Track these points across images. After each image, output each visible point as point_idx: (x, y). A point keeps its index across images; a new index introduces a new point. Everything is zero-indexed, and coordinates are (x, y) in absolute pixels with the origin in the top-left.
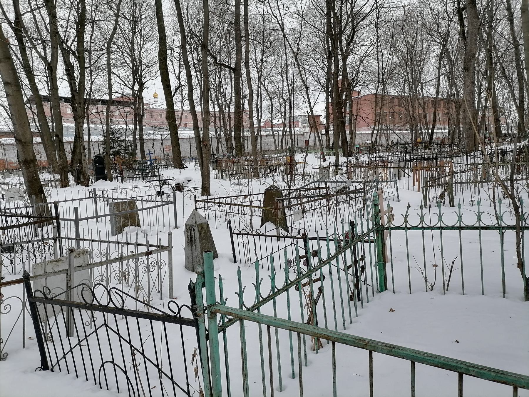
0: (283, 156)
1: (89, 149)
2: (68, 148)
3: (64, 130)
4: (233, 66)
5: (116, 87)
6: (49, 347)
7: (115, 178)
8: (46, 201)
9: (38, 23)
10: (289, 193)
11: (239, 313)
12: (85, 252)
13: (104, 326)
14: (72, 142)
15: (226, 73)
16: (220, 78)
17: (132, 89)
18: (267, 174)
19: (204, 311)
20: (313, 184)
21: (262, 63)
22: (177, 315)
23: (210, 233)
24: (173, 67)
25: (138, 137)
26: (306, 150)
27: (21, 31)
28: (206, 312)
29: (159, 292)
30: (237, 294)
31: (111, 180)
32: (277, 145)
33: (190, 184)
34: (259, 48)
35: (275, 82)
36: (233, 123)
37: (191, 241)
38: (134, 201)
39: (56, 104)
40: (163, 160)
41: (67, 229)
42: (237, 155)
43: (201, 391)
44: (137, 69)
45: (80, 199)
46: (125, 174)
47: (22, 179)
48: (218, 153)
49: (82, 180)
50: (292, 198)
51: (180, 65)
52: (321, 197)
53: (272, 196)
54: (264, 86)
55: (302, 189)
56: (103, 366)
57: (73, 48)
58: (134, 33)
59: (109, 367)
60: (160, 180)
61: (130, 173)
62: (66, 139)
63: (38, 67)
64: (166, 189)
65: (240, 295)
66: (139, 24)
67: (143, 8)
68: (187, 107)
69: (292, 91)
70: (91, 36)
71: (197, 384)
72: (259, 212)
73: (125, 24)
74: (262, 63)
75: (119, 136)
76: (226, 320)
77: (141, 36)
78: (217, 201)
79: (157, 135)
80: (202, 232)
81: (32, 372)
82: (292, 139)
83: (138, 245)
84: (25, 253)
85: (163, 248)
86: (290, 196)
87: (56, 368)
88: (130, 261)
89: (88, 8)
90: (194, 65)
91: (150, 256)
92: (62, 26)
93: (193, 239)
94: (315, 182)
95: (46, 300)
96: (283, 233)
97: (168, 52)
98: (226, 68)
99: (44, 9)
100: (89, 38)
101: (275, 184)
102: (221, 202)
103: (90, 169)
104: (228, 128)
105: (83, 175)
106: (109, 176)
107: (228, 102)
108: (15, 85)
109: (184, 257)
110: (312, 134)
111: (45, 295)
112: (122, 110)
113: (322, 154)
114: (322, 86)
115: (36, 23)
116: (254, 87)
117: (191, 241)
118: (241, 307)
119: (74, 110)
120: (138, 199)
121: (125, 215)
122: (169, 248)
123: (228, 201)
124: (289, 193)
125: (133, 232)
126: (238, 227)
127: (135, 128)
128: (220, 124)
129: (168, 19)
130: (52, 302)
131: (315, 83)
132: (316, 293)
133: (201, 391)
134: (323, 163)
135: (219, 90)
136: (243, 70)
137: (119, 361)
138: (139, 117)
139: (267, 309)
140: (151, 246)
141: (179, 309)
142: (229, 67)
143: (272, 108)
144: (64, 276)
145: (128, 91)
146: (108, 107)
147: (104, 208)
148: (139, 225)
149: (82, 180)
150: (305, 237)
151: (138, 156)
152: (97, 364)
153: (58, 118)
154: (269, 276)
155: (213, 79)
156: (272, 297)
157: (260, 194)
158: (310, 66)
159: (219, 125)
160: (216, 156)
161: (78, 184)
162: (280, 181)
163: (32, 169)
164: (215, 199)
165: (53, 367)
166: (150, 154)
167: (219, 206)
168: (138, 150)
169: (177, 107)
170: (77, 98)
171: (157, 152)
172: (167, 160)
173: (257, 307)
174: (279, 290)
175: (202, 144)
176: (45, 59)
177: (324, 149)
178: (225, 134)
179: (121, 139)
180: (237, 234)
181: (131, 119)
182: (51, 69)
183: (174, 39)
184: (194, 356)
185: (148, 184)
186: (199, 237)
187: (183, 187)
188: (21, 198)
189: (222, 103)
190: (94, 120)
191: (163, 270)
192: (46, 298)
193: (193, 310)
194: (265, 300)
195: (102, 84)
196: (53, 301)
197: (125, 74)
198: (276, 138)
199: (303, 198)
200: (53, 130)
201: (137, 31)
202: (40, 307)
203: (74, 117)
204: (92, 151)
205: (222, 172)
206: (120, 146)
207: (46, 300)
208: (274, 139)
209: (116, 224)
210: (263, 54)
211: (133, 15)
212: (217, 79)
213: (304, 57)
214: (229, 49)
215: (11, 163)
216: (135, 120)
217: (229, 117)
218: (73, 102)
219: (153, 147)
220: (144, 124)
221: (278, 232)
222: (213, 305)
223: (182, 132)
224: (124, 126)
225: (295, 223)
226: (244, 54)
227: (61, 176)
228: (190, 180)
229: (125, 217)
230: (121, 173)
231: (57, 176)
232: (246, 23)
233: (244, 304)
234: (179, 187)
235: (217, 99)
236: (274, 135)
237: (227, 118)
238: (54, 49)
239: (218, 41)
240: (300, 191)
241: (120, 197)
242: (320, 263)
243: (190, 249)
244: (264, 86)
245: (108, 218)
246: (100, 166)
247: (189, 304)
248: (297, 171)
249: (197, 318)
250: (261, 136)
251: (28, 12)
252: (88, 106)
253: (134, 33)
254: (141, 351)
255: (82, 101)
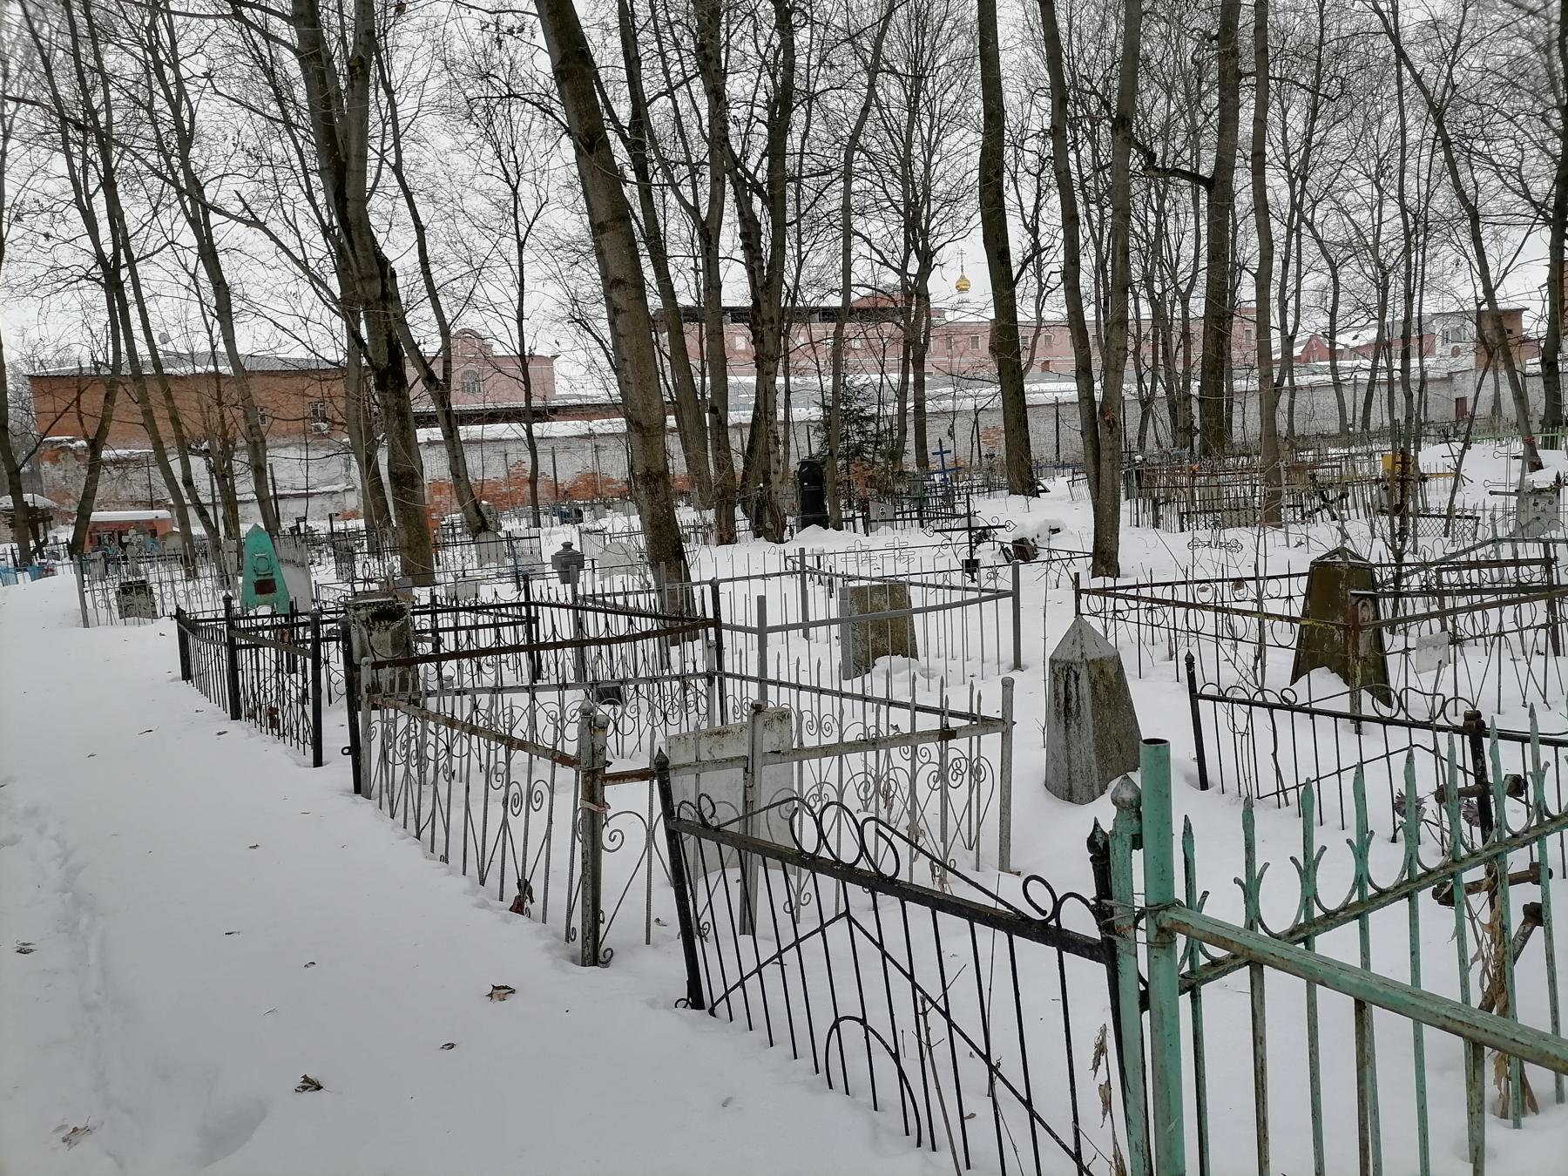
0: (1371, 455)
1: (787, 443)
2: (737, 442)
3: (730, 392)
4: (1205, 171)
5: (861, 270)
6: (707, 951)
7: (847, 520)
8: (688, 578)
9: (683, 120)
10: (1398, 578)
11: (1249, 940)
12: (784, 716)
13: (845, 919)
14: (746, 425)
15: (1182, 195)
16: (1160, 212)
17: (902, 271)
18: (1311, 514)
19: (1137, 920)
20: (1489, 547)
21: (1308, 151)
22: (1050, 919)
23: (1126, 690)
24: (1019, 195)
25: (910, 405)
26: (1464, 427)
27: (643, 146)
28: (1142, 923)
29: (971, 848)
30: (1241, 883)
31: (840, 528)
32: (1349, 416)
33: (1057, 542)
34: (1300, 99)
35: (1354, 204)
36: (1197, 353)
37: (1067, 709)
38: (903, 584)
39: (716, 327)
40: (979, 469)
41: (739, 652)
42: (1206, 452)
43: (1118, 1157)
44: (918, 214)
45: (764, 577)
46: (875, 510)
47: (636, 521)
48: (1142, 446)
49: (769, 525)
50: (1408, 594)
51: (1039, 188)
52: (1524, 592)
53: (1333, 582)
54: (1310, 226)
55: (1448, 563)
56: (836, 1025)
57: (761, 176)
58: (913, 110)
59: (852, 1031)
60: (970, 529)
61: (887, 508)
62: (734, 417)
63: (677, 229)
64: (987, 554)
65: (1250, 888)
66: (930, 85)
67: (944, 36)
68: (1056, 310)
69: (1418, 228)
70: (805, 135)
71: (1105, 1137)
72: (1286, 635)
73: (892, 91)
74: (1308, 151)
75: (863, 404)
76: (1203, 960)
77: (932, 116)
78: (1145, 592)
79: (963, 398)
80: (1100, 688)
81: (667, 1007)
82: (1409, 396)
83: (917, 709)
84: (644, 704)
85: (987, 724)
86: (1398, 585)
87: (722, 1008)
88: (894, 751)
89: (801, 60)
90: (1083, 180)
91: (951, 743)
92: (736, 122)
93: (1073, 705)
94: (1496, 541)
95: (705, 829)
96: (1368, 704)
97: (1009, 152)
98: (1182, 182)
99: (698, 80)
100: (797, 143)
101: (1348, 545)
102: (1158, 596)
103: (787, 497)
104: (1180, 367)
105: (772, 513)
106: (835, 517)
107: (1183, 288)
108: (634, 286)
109: (1042, 754)
110: (1489, 377)
111: (702, 816)
112: (872, 332)
113: (1530, 444)
114: (1539, 207)
115: (678, 118)
116: (1278, 229)
117: (1067, 709)
118: (1251, 926)
119: (758, 340)
120: (913, 579)
121: (879, 624)
122: (1003, 725)
123: (1181, 594)
124: (1398, 578)
125: (898, 672)
126: (1211, 676)
127: (905, 382)
128: (1155, 358)
129: (1013, 57)
130: (720, 837)
131: (1508, 197)
132: (1516, 919)
133: (1118, 1157)
134: (1530, 477)
135: (1157, 251)
136: (1242, 180)
137: (878, 1020)
138: (915, 354)
139: (1337, 945)
140: (953, 714)
141: (1057, 905)
142: (1194, 177)
143: (1336, 294)
144: (739, 772)
145: (891, 278)
146: (840, 327)
147: (823, 605)
148: (914, 655)
149: (769, 528)
150: (1475, 728)
151: (910, 461)
152: (823, 1023)
153: (718, 363)
154: (1349, 842)
155: (1143, 221)
156: (1358, 910)
157: (1289, 576)
158: (1488, 140)
159: (1149, 362)
160: (1139, 457)
161: (758, 535)
162: (1368, 540)
163: (661, 496)
164: (1138, 587)
165: (714, 1005)
166: (942, 453)
167: (1151, 609)
168: (910, 446)
169: (1025, 312)
170: (764, 306)
171: (962, 447)
172: (991, 469)
173: (1303, 933)
174: (1382, 893)
175: (1099, 420)
176: (694, 211)
177: (1535, 427)
178: (1169, 391)
179: (868, 412)
180: (1214, 699)
181: (894, 357)
182: (708, 234)
183: (1028, 111)
184: (1101, 1049)
185: (939, 538)
186: (1090, 697)
187: (1035, 548)
188: (629, 569)
189: (1165, 291)
190: (802, 364)
191: (985, 787)
192: (705, 825)
193: (1101, 912)
194: (1332, 919)
195: (823, 266)
196: (718, 834)
197: (884, 231)
198: (1347, 394)
199: (1454, 594)
200: (703, 395)
201: (921, 103)
202: (689, 842)
203: (756, 358)
204: (793, 449)
205: (1156, 504)
206: (864, 433)
207: (705, 829)
208: (1340, 396)
209: (854, 648)
210: (1314, 119)
211: (915, 60)
212: (1152, 217)
213: (1471, 111)
214: (1194, 121)
215: (610, 481)
216: (906, 360)
217: (1186, 335)
218: (754, 317)
219: (951, 434)
220: (928, 367)
221: (1356, 702)
222: (1167, 908)
223: (1035, 388)
224: (876, 377)
225: (1413, 673)
226: (1246, 127)
227: (718, 516)
228: (1058, 530)
229: (880, 629)
230: (864, 506)
231: (710, 515)
232: (1261, 28)
233: (1260, 920)
234: (1023, 551)
235: (1148, 280)
236: (1337, 385)
237: (1176, 338)
238: (717, 181)
239: (1162, 101)
240: (1439, 571)
241: (864, 572)
242: (1540, 819)
243: (1062, 732)
244: (1310, 226)
245: (835, 629)
246: (813, 488)
247: (1090, 893)
248: (1424, 502)
249: (1115, 937)
250: (1294, 389)
251: (660, 94)
252: (789, 327)
253: (913, 110)
254: (941, 1004)
255: (775, 314)
